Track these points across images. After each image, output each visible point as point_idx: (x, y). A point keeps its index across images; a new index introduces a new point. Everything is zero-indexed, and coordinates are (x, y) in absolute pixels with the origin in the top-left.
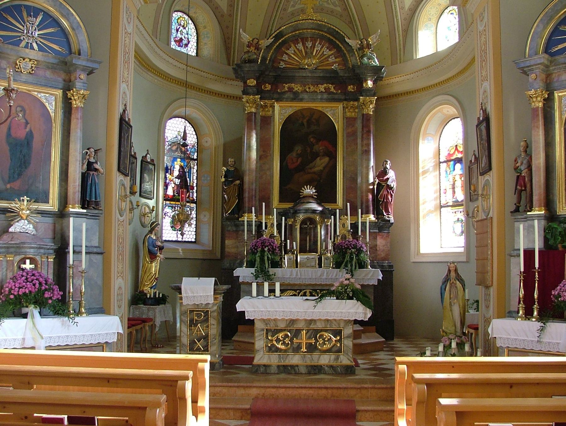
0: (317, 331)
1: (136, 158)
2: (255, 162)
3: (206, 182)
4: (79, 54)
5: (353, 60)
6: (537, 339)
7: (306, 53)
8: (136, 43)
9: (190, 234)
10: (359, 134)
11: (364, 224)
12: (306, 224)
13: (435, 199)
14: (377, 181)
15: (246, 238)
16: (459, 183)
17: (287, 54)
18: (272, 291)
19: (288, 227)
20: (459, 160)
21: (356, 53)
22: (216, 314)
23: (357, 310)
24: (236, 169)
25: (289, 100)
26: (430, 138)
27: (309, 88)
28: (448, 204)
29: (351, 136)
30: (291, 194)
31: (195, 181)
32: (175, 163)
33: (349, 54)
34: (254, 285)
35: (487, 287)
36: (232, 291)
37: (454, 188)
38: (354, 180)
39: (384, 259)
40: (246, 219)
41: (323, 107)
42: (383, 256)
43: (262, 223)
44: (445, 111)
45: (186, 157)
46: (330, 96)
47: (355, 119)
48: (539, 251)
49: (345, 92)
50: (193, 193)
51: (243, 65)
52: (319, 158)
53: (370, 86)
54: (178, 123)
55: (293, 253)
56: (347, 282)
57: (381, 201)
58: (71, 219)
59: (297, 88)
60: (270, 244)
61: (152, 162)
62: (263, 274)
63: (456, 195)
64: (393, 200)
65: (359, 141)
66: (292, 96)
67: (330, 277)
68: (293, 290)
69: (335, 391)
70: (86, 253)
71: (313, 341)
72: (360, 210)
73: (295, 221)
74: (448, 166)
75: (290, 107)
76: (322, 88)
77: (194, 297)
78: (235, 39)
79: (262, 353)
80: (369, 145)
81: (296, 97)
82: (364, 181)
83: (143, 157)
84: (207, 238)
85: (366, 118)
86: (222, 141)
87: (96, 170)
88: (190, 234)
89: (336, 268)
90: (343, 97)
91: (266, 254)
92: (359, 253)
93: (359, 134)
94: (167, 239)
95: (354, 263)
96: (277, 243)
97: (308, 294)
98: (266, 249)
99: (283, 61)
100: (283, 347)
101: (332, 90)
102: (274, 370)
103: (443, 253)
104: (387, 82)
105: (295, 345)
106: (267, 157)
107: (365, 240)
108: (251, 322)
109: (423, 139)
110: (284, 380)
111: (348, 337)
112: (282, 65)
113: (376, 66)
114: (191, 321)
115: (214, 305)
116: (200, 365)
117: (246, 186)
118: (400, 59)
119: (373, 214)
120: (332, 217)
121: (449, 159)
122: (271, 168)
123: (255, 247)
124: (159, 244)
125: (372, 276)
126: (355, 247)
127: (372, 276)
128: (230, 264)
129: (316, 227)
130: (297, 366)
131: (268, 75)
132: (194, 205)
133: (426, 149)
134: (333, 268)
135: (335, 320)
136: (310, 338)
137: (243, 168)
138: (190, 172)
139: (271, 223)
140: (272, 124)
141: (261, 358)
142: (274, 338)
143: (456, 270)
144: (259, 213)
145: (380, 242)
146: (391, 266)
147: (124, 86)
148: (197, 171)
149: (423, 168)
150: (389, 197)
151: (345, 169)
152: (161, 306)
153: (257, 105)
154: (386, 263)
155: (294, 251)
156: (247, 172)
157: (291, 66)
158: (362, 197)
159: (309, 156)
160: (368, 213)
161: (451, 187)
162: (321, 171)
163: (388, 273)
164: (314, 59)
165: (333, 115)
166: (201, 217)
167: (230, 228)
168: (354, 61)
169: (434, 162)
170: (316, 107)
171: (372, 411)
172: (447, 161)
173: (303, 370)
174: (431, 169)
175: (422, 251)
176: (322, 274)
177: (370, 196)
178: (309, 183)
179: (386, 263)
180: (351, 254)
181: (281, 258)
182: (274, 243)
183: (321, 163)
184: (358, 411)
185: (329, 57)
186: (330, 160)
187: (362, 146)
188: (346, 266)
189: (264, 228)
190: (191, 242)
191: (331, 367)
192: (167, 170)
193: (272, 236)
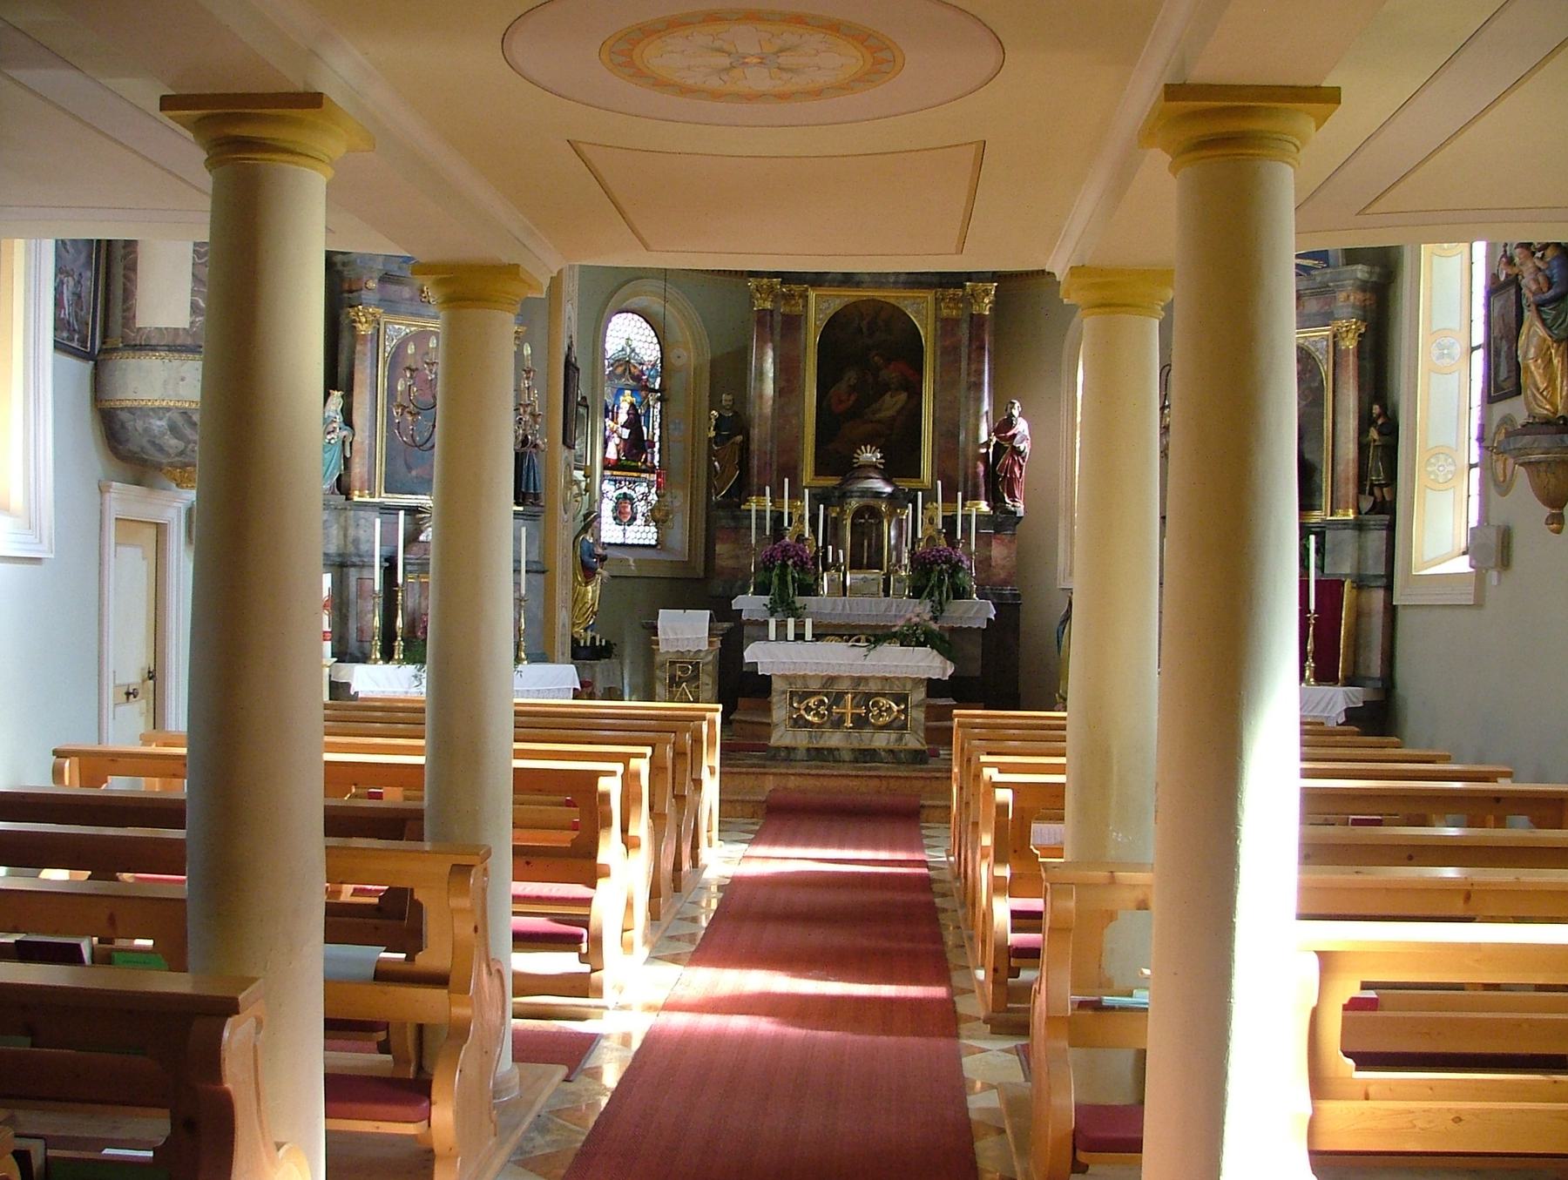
0: (869, 696)
10: (964, 351)
11: (966, 518)
14: (995, 439)
18: (800, 637)
23: (929, 664)
24: (735, 413)
29: (949, 354)
30: (836, 460)
31: (657, 432)
36: (733, 636)
39: (1005, 583)
40: (754, 507)
55: (838, 570)
62: (784, 606)
69: (892, 782)
71: (863, 711)
73: (843, 511)
75: (838, 296)
80: (981, 373)
84: (679, 536)
85: (977, 322)
86: (709, 357)
88: (642, 533)
93: (964, 351)
96: (809, 551)
100: (816, 720)
105: (835, 717)
108: (767, 680)
114: (672, 678)
117: (754, 446)
122: (800, 413)
123: (771, 558)
124: (600, 551)
125: (977, 612)
126: (948, 560)
136: (858, 706)
139: (800, 514)
141: (781, 736)
144: (777, 495)
145: (998, 551)
154: (1007, 591)
158: (966, 467)
160: (976, 497)
162: (893, 418)
163: (1009, 610)
165: (917, 312)
167: (724, 522)
173: (847, 756)
177: (981, 468)
179: (1007, 591)
183: (892, 404)
184: (923, 806)
188: (931, 595)
191: (891, 751)
192: (609, 412)
193: (800, 538)
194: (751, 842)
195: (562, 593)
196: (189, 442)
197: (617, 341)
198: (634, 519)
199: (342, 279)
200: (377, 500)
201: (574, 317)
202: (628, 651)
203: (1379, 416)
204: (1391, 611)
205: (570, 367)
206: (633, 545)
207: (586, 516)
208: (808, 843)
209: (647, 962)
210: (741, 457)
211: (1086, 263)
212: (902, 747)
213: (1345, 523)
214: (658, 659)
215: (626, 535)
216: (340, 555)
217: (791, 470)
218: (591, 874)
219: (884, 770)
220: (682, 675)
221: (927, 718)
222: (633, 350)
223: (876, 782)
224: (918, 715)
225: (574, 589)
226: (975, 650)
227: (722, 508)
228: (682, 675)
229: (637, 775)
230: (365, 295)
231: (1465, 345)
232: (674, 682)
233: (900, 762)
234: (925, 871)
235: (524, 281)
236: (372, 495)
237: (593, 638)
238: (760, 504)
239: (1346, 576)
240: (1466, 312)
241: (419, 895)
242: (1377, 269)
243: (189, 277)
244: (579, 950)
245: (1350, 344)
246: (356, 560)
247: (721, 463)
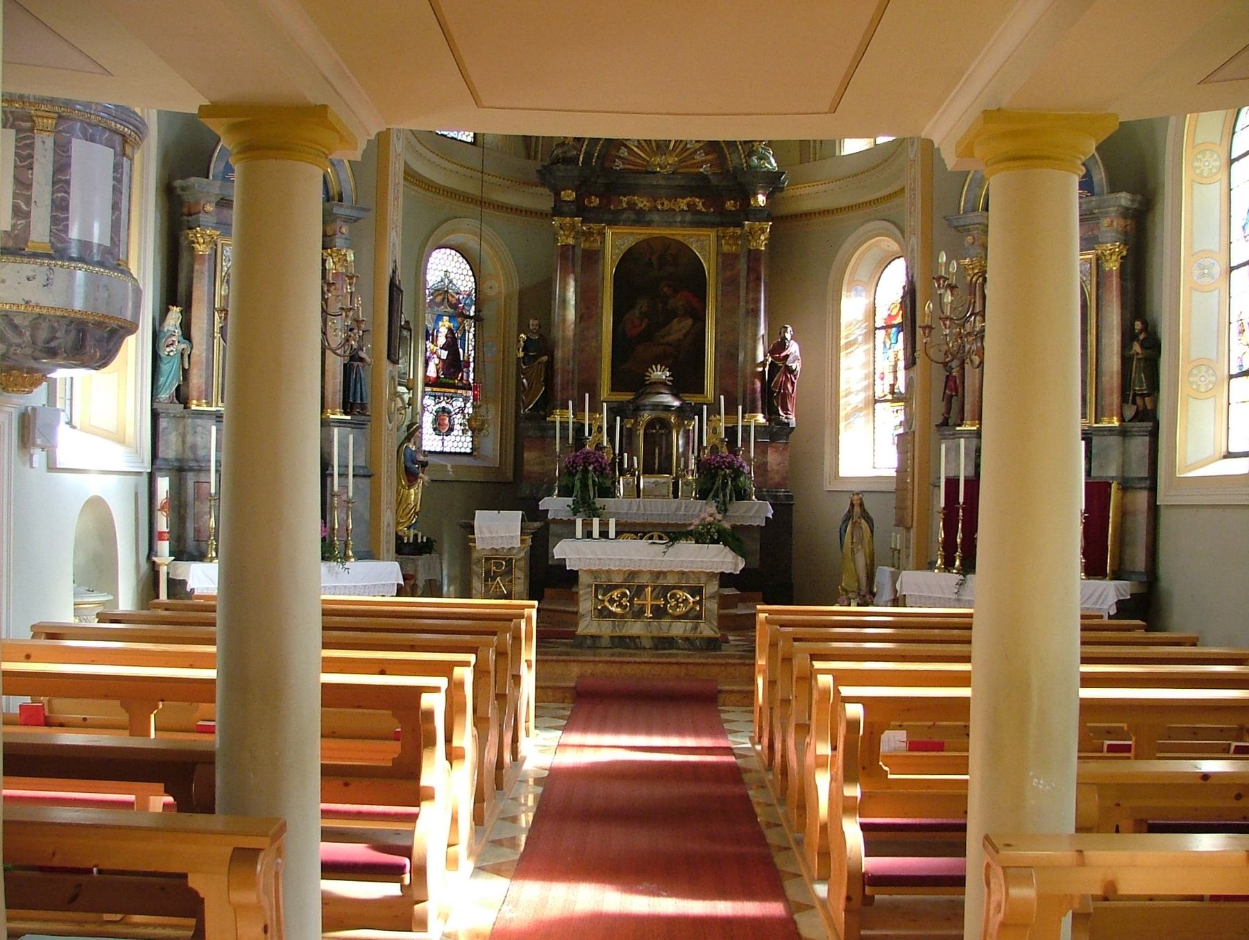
0: (667, 589)
4: (341, 200)
6: (954, 597)
8: (405, 163)
10: (743, 283)
11: (746, 429)
13: (866, 388)
18: (604, 534)
27: (662, 204)
29: (729, 285)
30: (630, 378)
34: (579, 522)
35: (908, 529)
36: (541, 535)
39: (779, 485)
40: (558, 419)
41: (684, 235)
43: (583, 425)
45: (457, 313)
47: (735, 256)
48: (965, 481)
49: (722, 212)
55: (633, 475)
56: (710, 519)
58: (336, 430)
59: (642, 203)
60: (597, 461)
61: (407, 327)
62: (586, 507)
65: (742, 293)
66: (633, 217)
70: (354, 476)
72: (740, 407)
73: (637, 423)
74: (888, 335)
76: (683, 204)
79: (588, 618)
80: (758, 301)
81: (640, 218)
82: (749, 358)
84: (491, 445)
85: (754, 256)
86: (517, 287)
87: (362, 360)
88: (459, 442)
89: (700, 499)
90: (718, 219)
93: (743, 283)
96: (608, 457)
97: (656, 535)
101: (700, 206)
102: (605, 642)
104: (791, 193)
105: (636, 608)
108: (574, 574)
110: (620, 655)
111: (712, 597)
112: (619, 165)
114: (488, 572)
115: (520, 549)
116: (526, 611)
117: (558, 365)
122: (598, 336)
123: (574, 464)
124: (421, 458)
125: (757, 511)
126: (731, 465)
127: (758, 511)
129: (671, 432)
130: (639, 637)
133: (852, 307)
135: (693, 573)
136: (657, 598)
139: (599, 425)
141: (588, 626)
142: (607, 598)
143: (861, 505)
144: (579, 408)
145: (773, 458)
147: (393, 233)
149: (846, 337)
152: (424, 556)
153: (577, 233)
154: (781, 492)
158: (745, 385)
159: (661, 316)
163: (784, 508)
165: (702, 249)
171: (739, 692)
172: (887, 327)
173: (647, 643)
174: (860, 339)
175: (844, 471)
176: (678, 509)
177: (758, 384)
178: (660, 360)
179: (781, 492)
181: (614, 483)
184: (720, 692)
185: (695, 152)
188: (716, 496)
190: (465, 454)
191: (687, 639)
192: (430, 336)
193: (599, 447)
194: (565, 729)
195: (387, 495)
196: (10, 345)
197: (437, 273)
198: (451, 430)
199: (182, 203)
200: (214, 409)
201: (398, 242)
202: (446, 546)
203: (1141, 331)
204: (1154, 509)
205: (394, 289)
207: (409, 427)
208: (618, 729)
209: (474, 874)
211: (1003, 106)
212: (698, 635)
213: (1111, 431)
214: (475, 555)
215: (446, 439)
216: (178, 460)
217: (591, 386)
218: (417, 795)
219: (681, 656)
220: (496, 570)
221: (719, 608)
222: (451, 282)
223: (675, 668)
224: (712, 605)
225: (398, 492)
226: (754, 546)
228: (496, 570)
229: (461, 685)
230: (203, 218)
231: (1225, 266)
232: (489, 577)
233: (696, 649)
234: (731, 759)
235: (331, 127)
236: (209, 404)
237: (416, 536)
238: (563, 417)
239: (1112, 478)
240: (1225, 233)
241: (194, 882)
242: (1139, 198)
243: (10, 180)
244: (401, 881)
245: (1113, 266)
246: (192, 464)
247: (527, 379)
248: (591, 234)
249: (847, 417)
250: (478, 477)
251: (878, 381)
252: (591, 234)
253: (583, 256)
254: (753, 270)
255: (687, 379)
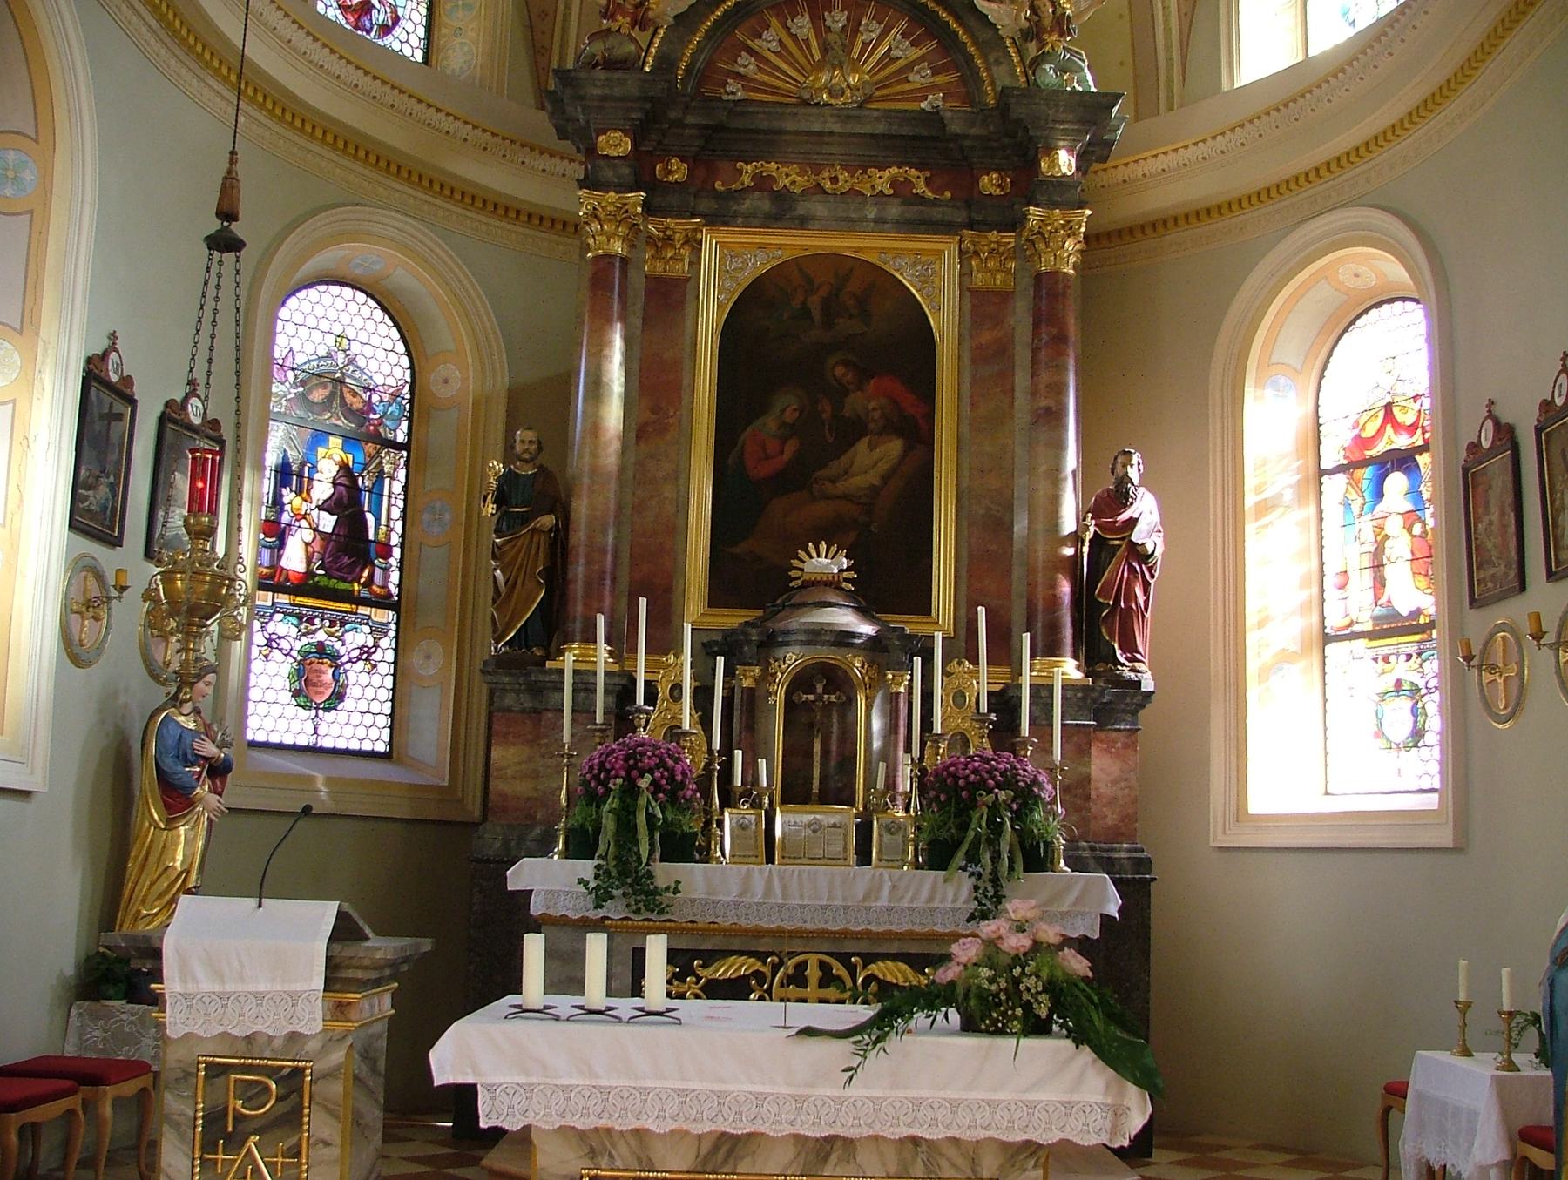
1: (132, 402)
2: (615, 446)
3: (436, 530)
5: (998, 77)
7: (825, 49)
9: (360, 721)
10: (1022, 355)
12: (812, 690)
13: (1304, 609)
15: (566, 737)
16: (1400, 546)
17: (752, 52)
19: (737, 700)
20: (1403, 461)
21: (1012, 51)
22: (337, 1088)
24: (542, 469)
25: (756, 222)
26: (1282, 380)
27: (834, 180)
28: (1356, 628)
29: (989, 358)
30: (753, 576)
31: (398, 526)
32: (321, 451)
33: (985, 57)
37: (1378, 566)
38: (1000, 525)
39: (1116, 835)
41: (883, 251)
42: (1109, 822)
43: (634, 681)
44: (1345, 275)
45: (366, 433)
46: (913, 212)
47: (1005, 297)
49: (970, 199)
50: (386, 570)
51: (583, 75)
52: (866, 440)
53: (1065, 170)
54: (340, 303)
55: (755, 804)
57: (1102, 606)
59: (788, 177)
62: (630, 892)
63: (1389, 590)
64: (1157, 607)
65: (1021, 379)
66: (766, 205)
67: (905, 904)
68: (750, 954)
72: (1026, 637)
73: (767, 677)
74: (1355, 484)
75: (761, 247)
76: (882, 180)
77: (224, 997)
78: (566, 17)
80: (1060, 390)
81: (783, 210)
82: (1040, 526)
83: (168, 404)
85: (1047, 287)
86: (502, 381)
88: (360, 721)
91: (642, 801)
92: (1024, 805)
93: (1022, 355)
94: (261, 737)
95: (1004, 848)
96: (693, 760)
98: (644, 783)
99: (739, 76)
101: (921, 188)
103: (1345, 813)
106: (664, 429)
107: (1048, 758)
109: (1259, 384)
113: (1087, 93)
114: (215, 1118)
117: (579, 537)
118: (1170, 98)
119: (1075, 656)
120: (917, 660)
121: (1357, 456)
123: (601, 772)
124: (210, 749)
126: (1009, 782)
128: (506, 842)
129: (852, 701)
131: (680, 124)
132: (388, 616)
133: (1270, 420)
134: (918, 867)
135: (955, 1141)
137: (570, 472)
138: (377, 490)
140: (689, 309)
144: (621, 642)
145: (1102, 767)
146: (1143, 864)
148: (406, 488)
149: (1258, 490)
150: (1138, 591)
151: (964, 485)
154: (1122, 851)
155: (760, 797)
156: (586, 480)
157: (766, 98)
158: (1032, 586)
159: (829, 434)
161: (1366, 561)
162: (874, 491)
164: (855, 70)
165: (925, 281)
166: (415, 659)
168: (1004, 80)
169: (1299, 471)
170: (858, 250)
174: (1288, 495)
175: (1260, 801)
176: (873, 892)
177: (1065, 588)
178: (828, 533)
180: (994, 809)
181: (708, 823)
182: (677, 760)
183: (872, 461)
185: (910, 67)
186: (908, 449)
187: (1034, 393)
188: (973, 858)
189: (640, 700)
190: (372, 755)
193: (675, 733)
206: (334, 752)
210: (552, 555)
227: (515, 670)
248: (668, 240)
249: (1265, 673)
250: (401, 809)
251: (1331, 594)
252: (668, 240)
253: (649, 293)
254: (1047, 316)
255: (892, 581)
